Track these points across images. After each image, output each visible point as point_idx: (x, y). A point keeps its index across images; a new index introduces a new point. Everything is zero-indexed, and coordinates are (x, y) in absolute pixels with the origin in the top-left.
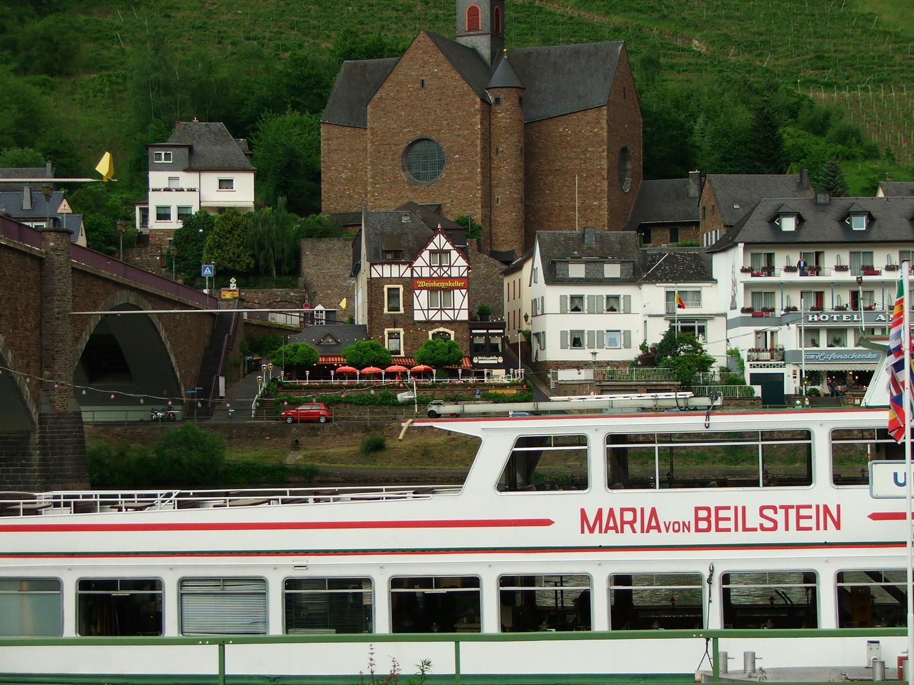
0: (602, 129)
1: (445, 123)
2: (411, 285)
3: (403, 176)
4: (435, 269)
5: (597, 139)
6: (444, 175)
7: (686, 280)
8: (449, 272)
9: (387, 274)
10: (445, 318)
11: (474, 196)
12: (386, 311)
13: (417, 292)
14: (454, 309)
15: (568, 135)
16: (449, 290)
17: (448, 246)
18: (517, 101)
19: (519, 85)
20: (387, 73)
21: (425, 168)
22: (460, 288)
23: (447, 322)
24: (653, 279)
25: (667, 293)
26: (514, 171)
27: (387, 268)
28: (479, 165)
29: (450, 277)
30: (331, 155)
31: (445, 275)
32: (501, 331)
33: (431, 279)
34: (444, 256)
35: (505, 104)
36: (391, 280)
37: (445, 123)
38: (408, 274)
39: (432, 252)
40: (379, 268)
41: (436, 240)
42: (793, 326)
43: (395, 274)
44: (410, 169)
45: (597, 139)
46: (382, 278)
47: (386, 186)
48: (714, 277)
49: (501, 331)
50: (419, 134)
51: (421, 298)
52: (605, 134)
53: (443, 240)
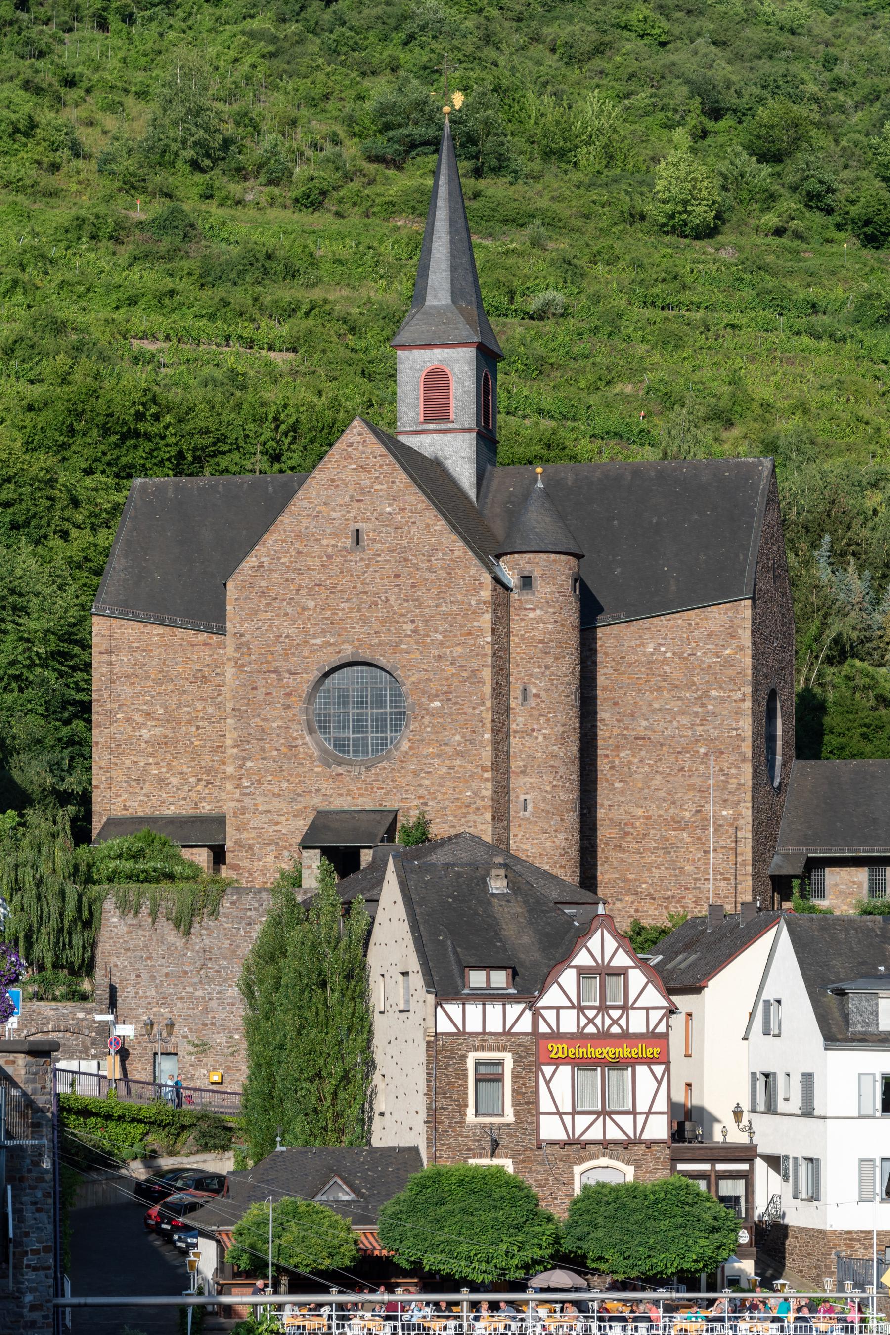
0: (741, 648)
2: (534, 1052)
3: (309, 744)
4: (591, 1013)
5: (731, 672)
6: (405, 745)
9: (474, 1025)
10: (614, 1134)
11: (475, 794)
12: (470, 1116)
13: (548, 1070)
14: (634, 1112)
15: (665, 661)
17: (622, 959)
19: (577, 551)
21: (359, 727)
22: (649, 1062)
23: (616, 1143)
26: (562, 740)
28: (489, 726)
29: (625, 1035)
31: (615, 1030)
32: (745, 1167)
33: (580, 1037)
34: (611, 980)
35: (543, 589)
36: (483, 1039)
37: (409, 627)
39: (582, 971)
40: (454, 1009)
41: (594, 943)
43: (495, 1025)
44: (325, 729)
45: (731, 672)
46: (462, 1034)
50: (347, 652)
51: (559, 1085)
52: (748, 661)
53: (611, 944)
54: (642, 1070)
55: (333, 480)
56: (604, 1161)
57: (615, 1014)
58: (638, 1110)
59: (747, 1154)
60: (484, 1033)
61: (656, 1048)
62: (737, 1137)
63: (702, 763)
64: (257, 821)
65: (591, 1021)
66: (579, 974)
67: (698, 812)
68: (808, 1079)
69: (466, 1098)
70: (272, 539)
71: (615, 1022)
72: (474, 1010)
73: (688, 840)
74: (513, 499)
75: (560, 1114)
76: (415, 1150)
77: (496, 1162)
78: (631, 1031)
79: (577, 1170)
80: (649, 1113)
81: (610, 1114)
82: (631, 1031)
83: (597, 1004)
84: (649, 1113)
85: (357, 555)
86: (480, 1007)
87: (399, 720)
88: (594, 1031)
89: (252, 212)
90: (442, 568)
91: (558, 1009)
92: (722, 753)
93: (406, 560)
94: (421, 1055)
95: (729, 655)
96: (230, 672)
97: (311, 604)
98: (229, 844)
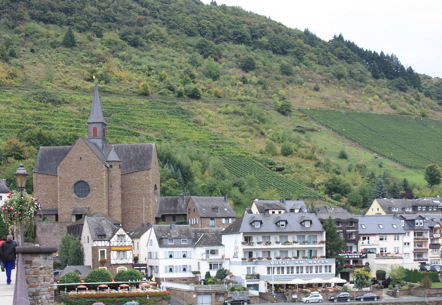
0: (149, 177)
1: (90, 175)
2: (110, 249)
3: (74, 195)
5: (148, 182)
6: (90, 196)
7: (213, 246)
9: (100, 245)
10: (123, 262)
11: (103, 204)
13: (112, 252)
15: (137, 180)
16: (124, 251)
17: (124, 233)
18: (118, 167)
19: (120, 160)
20: (64, 154)
22: (129, 250)
24: (200, 244)
27: (100, 242)
29: (125, 246)
30: (38, 185)
31: (123, 245)
32: (145, 267)
33: (117, 246)
36: (101, 247)
38: (108, 245)
39: (118, 236)
41: (120, 230)
42: (121, 222)
43: (103, 245)
45: (148, 182)
47: (66, 199)
49: (145, 267)
50: (79, 179)
51: (114, 255)
53: (122, 230)
59: (145, 265)
61: (131, 248)
62: (144, 262)
64: (64, 209)
68: (156, 252)
70: (65, 159)
76: (90, 266)
77: (104, 267)
79: (118, 268)
85: (81, 162)
87: (89, 191)
89: (169, 78)
94: (91, 250)
96: (58, 183)
98: (59, 214)
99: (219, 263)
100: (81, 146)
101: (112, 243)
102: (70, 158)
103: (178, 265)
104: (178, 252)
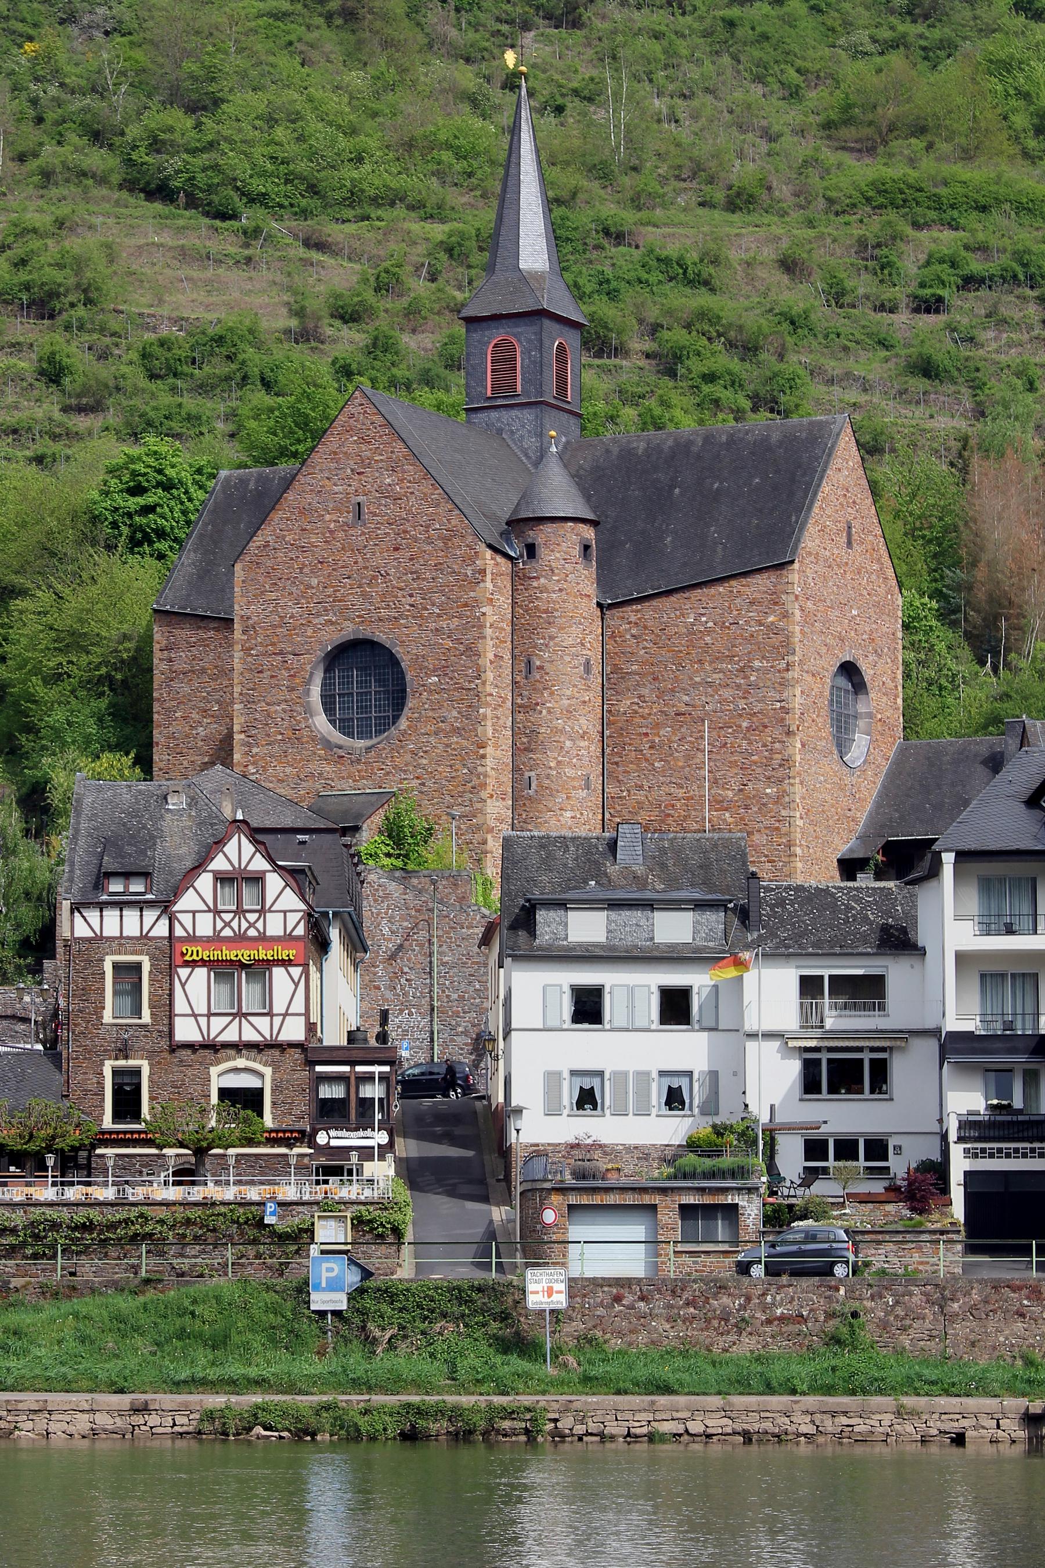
2: (171, 956)
4: (227, 917)
5: (775, 640)
8: (260, 925)
9: (111, 928)
10: (250, 1035)
13: (183, 972)
14: (270, 1014)
15: (709, 631)
17: (259, 864)
19: (591, 516)
22: (286, 963)
25: (804, 980)
29: (263, 938)
31: (252, 932)
33: (216, 939)
36: (121, 942)
39: (222, 879)
40: (93, 916)
45: (775, 640)
48: (920, 944)
51: (195, 987)
53: (248, 848)
54: (278, 972)
55: (335, 453)
56: (241, 1062)
57: (252, 917)
58: (275, 1011)
60: (121, 937)
63: (743, 738)
65: (227, 924)
66: (216, 879)
67: (741, 790)
69: (102, 1001)
71: (251, 925)
72: (111, 916)
73: (730, 820)
74: (582, 472)
75: (195, 1016)
77: (131, 1062)
78: (268, 934)
79: (214, 1071)
80: (286, 1014)
81: (246, 1015)
82: (268, 934)
83: (234, 908)
84: (286, 1014)
86: (118, 913)
88: (231, 934)
90: (440, 538)
91: (194, 912)
92: (766, 727)
93: (405, 532)
95: (772, 623)
97: (314, 582)
99: (866, 1057)
100: (363, 440)
101: (186, 919)
102: (303, 512)
103: (631, 1066)
104: (631, 990)
